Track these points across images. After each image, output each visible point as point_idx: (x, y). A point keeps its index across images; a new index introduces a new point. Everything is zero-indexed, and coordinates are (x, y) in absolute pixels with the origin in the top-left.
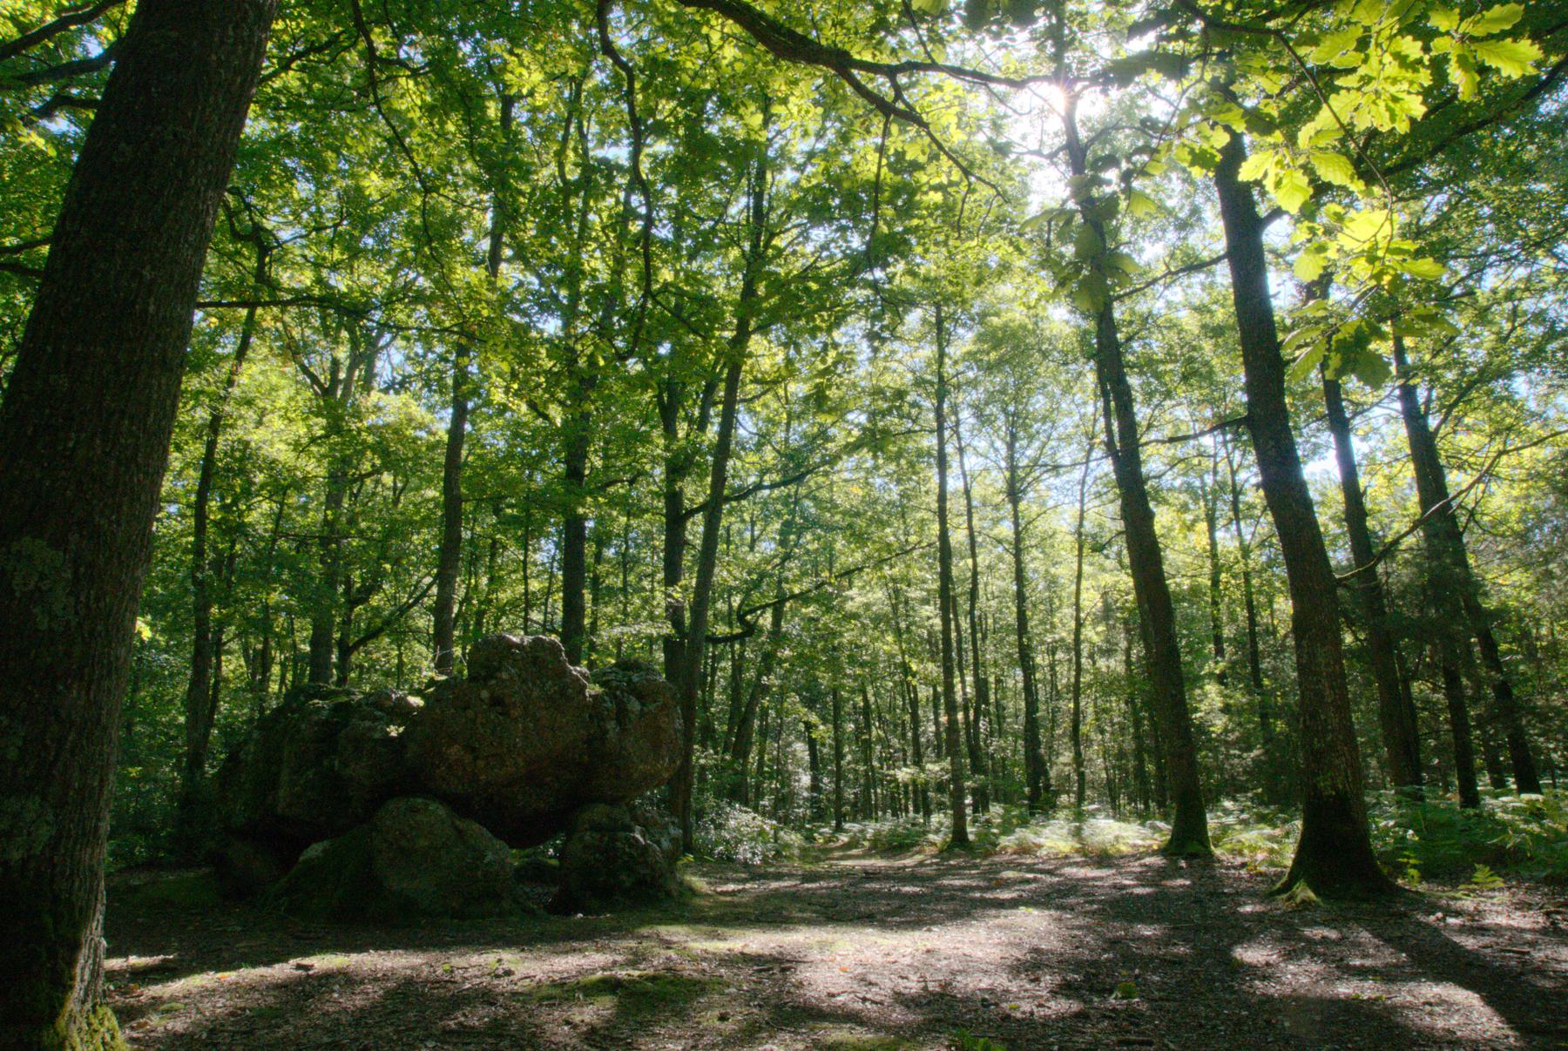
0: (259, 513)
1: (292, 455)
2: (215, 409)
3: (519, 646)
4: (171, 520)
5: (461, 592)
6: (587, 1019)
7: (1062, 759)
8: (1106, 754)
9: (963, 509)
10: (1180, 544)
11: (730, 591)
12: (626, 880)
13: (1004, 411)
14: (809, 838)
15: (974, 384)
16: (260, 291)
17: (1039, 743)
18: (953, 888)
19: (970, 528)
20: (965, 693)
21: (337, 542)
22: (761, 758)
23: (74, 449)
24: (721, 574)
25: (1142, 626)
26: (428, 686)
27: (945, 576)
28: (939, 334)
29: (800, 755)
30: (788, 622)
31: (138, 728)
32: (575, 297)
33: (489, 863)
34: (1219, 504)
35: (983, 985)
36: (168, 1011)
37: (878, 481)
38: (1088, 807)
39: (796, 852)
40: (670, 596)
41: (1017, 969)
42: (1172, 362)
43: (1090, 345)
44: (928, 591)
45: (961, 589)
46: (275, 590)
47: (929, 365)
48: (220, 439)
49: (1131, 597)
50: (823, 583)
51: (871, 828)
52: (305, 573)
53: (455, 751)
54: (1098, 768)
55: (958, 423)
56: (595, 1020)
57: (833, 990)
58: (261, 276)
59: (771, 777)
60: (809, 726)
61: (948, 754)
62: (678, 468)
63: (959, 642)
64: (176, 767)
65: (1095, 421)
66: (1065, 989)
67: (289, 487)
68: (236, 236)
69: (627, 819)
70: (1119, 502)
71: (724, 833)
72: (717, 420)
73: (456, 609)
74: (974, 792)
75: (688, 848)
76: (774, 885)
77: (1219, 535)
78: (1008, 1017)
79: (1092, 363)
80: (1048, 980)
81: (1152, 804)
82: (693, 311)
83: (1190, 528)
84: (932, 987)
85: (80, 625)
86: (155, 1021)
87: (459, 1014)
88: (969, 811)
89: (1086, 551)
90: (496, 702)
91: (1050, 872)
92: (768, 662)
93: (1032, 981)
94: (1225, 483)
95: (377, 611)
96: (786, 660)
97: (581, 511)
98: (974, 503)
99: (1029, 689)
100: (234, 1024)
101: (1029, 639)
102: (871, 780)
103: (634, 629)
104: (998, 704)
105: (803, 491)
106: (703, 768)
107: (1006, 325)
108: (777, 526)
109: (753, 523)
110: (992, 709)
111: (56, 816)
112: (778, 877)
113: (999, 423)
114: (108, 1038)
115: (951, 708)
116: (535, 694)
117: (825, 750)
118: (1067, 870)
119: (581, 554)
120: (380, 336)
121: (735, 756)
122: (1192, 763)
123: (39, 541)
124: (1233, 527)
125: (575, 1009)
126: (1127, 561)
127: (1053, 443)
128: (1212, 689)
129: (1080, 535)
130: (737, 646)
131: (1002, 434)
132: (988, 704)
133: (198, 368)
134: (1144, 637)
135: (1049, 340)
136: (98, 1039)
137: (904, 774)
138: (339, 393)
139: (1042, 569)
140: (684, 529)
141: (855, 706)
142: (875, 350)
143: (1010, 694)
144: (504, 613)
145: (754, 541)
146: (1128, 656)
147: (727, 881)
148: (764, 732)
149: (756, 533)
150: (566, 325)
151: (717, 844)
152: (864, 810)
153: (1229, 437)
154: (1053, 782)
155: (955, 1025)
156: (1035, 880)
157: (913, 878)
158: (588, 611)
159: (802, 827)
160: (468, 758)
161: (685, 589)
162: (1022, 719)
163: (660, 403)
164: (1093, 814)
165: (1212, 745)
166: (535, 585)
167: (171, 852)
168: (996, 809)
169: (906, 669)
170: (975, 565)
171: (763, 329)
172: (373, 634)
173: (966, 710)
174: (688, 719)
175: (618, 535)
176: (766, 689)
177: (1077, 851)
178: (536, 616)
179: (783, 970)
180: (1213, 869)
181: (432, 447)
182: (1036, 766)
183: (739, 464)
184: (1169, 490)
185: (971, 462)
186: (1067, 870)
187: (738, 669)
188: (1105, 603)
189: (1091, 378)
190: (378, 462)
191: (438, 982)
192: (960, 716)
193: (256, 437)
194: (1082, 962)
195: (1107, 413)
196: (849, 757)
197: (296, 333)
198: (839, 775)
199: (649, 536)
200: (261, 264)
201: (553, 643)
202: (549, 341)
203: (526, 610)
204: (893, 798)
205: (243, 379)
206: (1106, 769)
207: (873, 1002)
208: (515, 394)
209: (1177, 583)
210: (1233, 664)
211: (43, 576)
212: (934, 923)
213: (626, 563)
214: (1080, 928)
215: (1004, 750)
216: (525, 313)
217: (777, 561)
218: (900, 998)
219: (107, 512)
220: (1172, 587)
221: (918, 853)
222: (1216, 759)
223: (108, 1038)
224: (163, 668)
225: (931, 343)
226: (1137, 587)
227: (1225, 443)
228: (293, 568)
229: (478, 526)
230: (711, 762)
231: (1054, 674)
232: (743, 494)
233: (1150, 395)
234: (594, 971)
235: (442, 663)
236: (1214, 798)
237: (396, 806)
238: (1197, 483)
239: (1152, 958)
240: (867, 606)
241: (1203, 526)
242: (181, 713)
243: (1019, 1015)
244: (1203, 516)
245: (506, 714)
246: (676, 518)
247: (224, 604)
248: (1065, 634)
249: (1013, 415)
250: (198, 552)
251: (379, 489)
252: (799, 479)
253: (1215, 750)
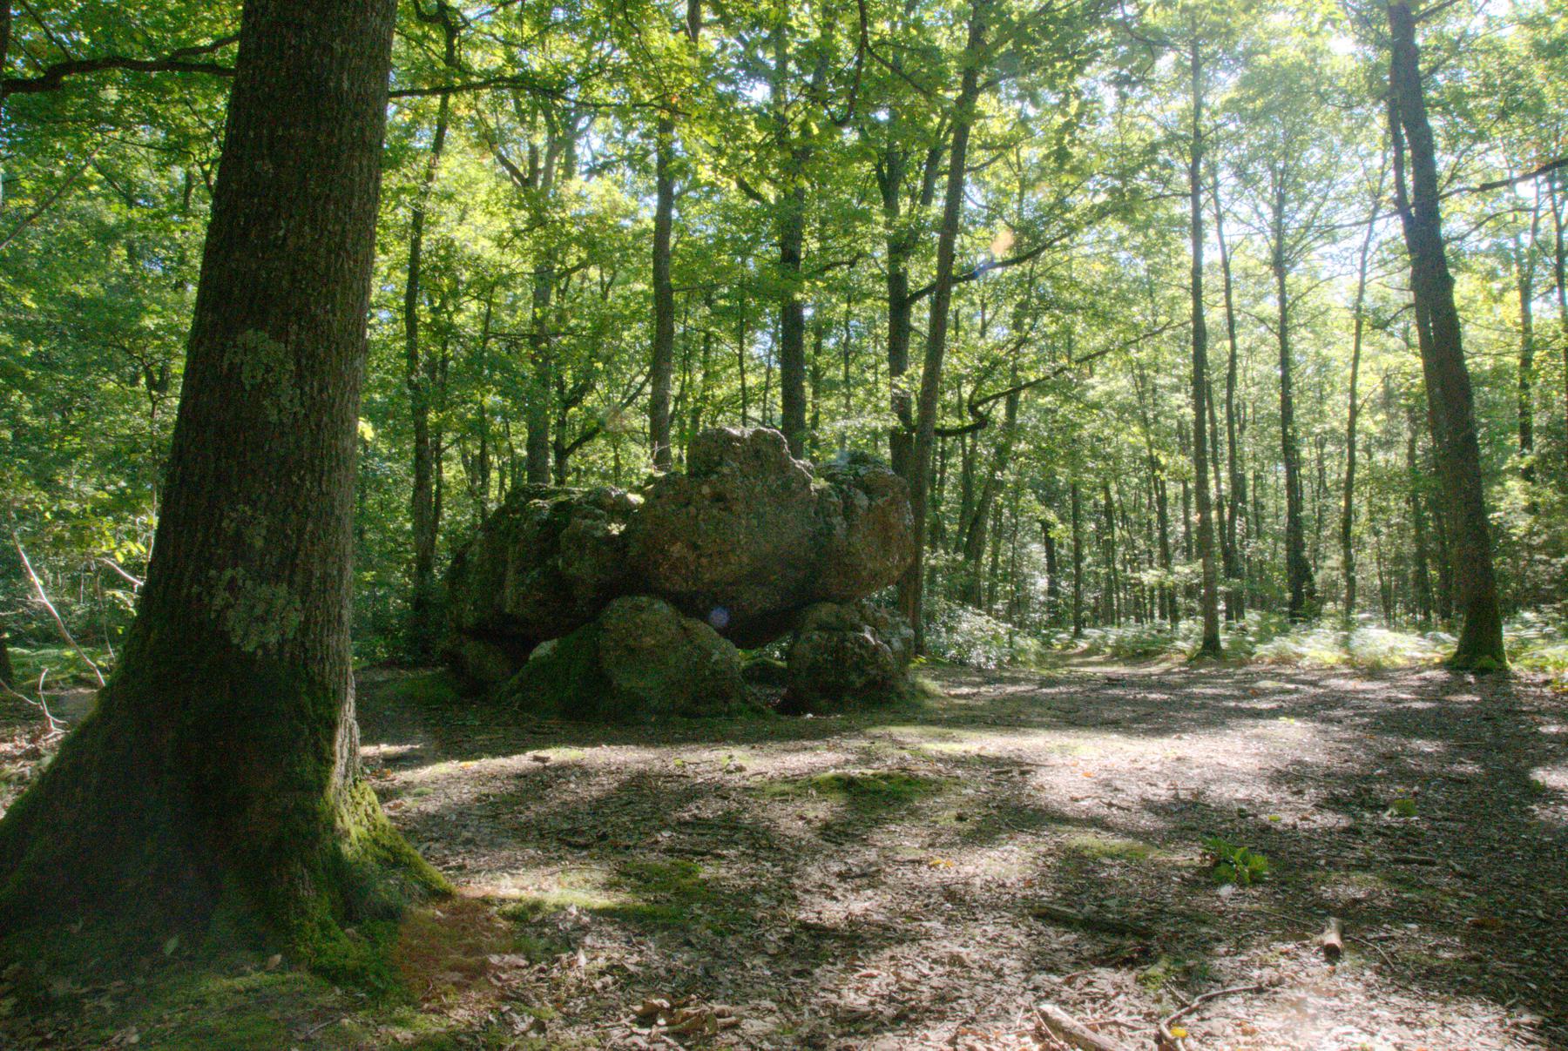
0: (468, 314)
1: (495, 251)
2: (418, 206)
3: (738, 439)
4: (383, 325)
5: (675, 390)
6: (821, 815)
7: (1329, 563)
8: (1381, 557)
9: (1221, 284)
10: (1484, 317)
11: (959, 380)
12: (858, 681)
13: (1272, 168)
14: (1047, 644)
15: (1236, 138)
16: (450, 78)
17: (1303, 546)
18: (1204, 696)
19: (1229, 305)
20: (1219, 490)
21: (548, 341)
22: (995, 560)
23: (285, 238)
24: (951, 363)
25: (1431, 414)
26: (647, 483)
27: (1199, 359)
28: (1195, 81)
29: (1035, 556)
30: (1023, 414)
31: (369, 536)
32: (783, 60)
33: (716, 663)
34: (1538, 269)
35: (1239, 796)
36: (419, 795)
37: (1123, 255)
38: (1357, 616)
39: (1032, 657)
40: (896, 386)
41: (1279, 778)
42: (1488, 95)
43: (1381, 82)
44: (1179, 377)
45: (1216, 375)
46: (489, 391)
47: (1183, 118)
48: (424, 239)
49: (1418, 381)
50: (1062, 369)
51: (1113, 634)
52: (517, 374)
53: (677, 549)
54: (1370, 574)
55: (1216, 185)
56: (829, 817)
57: (1076, 795)
58: (450, 59)
59: (1005, 580)
60: (1046, 526)
61: (1198, 557)
62: (901, 248)
63: (1214, 434)
64: (407, 573)
65: (1383, 174)
66: (1333, 803)
67: (496, 284)
68: (423, 18)
69: (857, 619)
70: (1410, 270)
71: (957, 637)
72: (942, 193)
73: (671, 408)
74: (1228, 597)
75: (920, 649)
76: (1010, 689)
77: (1535, 306)
78: (1269, 828)
79: (1382, 104)
80: (1311, 793)
81: (1433, 615)
82: (912, 68)
83: (1498, 298)
84: (1183, 795)
85: (306, 416)
86: (408, 802)
87: (692, 806)
88: (1221, 617)
89: (1365, 327)
90: (718, 498)
91: (1314, 684)
92: (1002, 456)
93: (1295, 793)
94: (1548, 243)
95: (591, 412)
96: (1022, 454)
97: (798, 296)
98: (1233, 277)
99: (1293, 487)
100: (479, 808)
101: (1295, 430)
102: (1113, 584)
103: (856, 422)
104: (1258, 505)
105: (1039, 269)
106: (934, 569)
107: (1276, 64)
108: (1011, 309)
109: (984, 306)
110: (1249, 508)
111: (303, 603)
112: (1014, 681)
113: (1263, 184)
114: (370, 811)
115: (1204, 506)
116: (758, 489)
117: (1063, 552)
118: (1333, 682)
119: (799, 344)
120: (576, 120)
121: (968, 557)
122: (1488, 568)
123: (260, 333)
124: (1555, 296)
125: (808, 805)
126: (1415, 339)
127: (1328, 204)
128: (1514, 485)
129: (1359, 309)
130: (968, 440)
131: (1268, 196)
132: (1244, 502)
133: (395, 164)
134: (1433, 428)
135: (1330, 79)
136: (361, 811)
137: (1150, 577)
138: (540, 183)
139: (1312, 350)
140: (909, 314)
141: (1096, 505)
142: (1124, 97)
143: (1270, 491)
144: (721, 411)
145: (985, 326)
146: (1412, 448)
147: (961, 684)
148: (998, 533)
149: (988, 317)
150: (776, 90)
151: (948, 648)
152: (1106, 615)
153: (1557, 185)
154: (1318, 587)
155: (1209, 834)
156: (1296, 691)
157: (1161, 685)
158: (809, 406)
159: (1039, 633)
160: (691, 556)
161: (911, 379)
162: (1284, 519)
163: (880, 176)
164: (1363, 624)
165: (1511, 549)
166: (752, 380)
167: (409, 653)
168: (1252, 617)
169: (1154, 463)
170: (1234, 348)
171: (991, 85)
172: (588, 436)
173: (1220, 507)
174: (919, 514)
175: (839, 323)
176: (1000, 485)
177: (1345, 662)
178: (753, 412)
179: (1023, 773)
180: (1508, 685)
181: (638, 236)
182: (1299, 571)
183: (967, 241)
184: (1474, 254)
185: (1231, 229)
186: (1333, 682)
187: (969, 464)
188: (1387, 387)
189: (1380, 123)
190: (584, 255)
191: (670, 777)
192: (1214, 514)
193: (461, 234)
194: (1352, 776)
195: (1399, 165)
196: (1089, 559)
197: (492, 123)
198: (1078, 578)
199: (871, 323)
200: (450, 47)
201: (774, 436)
202: (758, 110)
203: (743, 406)
204: (1137, 604)
205: (442, 173)
206: (1380, 575)
207: (1119, 808)
208: (724, 171)
209: (1478, 363)
210: (1543, 458)
211: (268, 369)
212: (1184, 731)
213: (847, 353)
214: (1348, 741)
215: (1262, 552)
216: (729, 80)
217: (1011, 346)
218: (1149, 806)
219: (322, 302)
220: (1471, 368)
221: (1163, 660)
222: (1515, 565)
223: (370, 811)
224: (387, 477)
225: (1185, 92)
226: (1427, 368)
227: (1552, 192)
228: (505, 369)
229: (691, 319)
230: (941, 563)
231: (1322, 471)
232: (971, 275)
233: (1453, 140)
234: (826, 769)
235: (661, 459)
236: (1512, 607)
237: (620, 605)
238: (1511, 245)
239: (1433, 775)
240: (1110, 395)
241: (1514, 296)
242: (409, 521)
243: (1280, 827)
244: (1515, 284)
245: (728, 509)
246: (900, 303)
247: (441, 408)
248: (1338, 424)
249: (1282, 172)
250: (411, 355)
251: (586, 285)
252: (1033, 255)
253: (1514, 556)
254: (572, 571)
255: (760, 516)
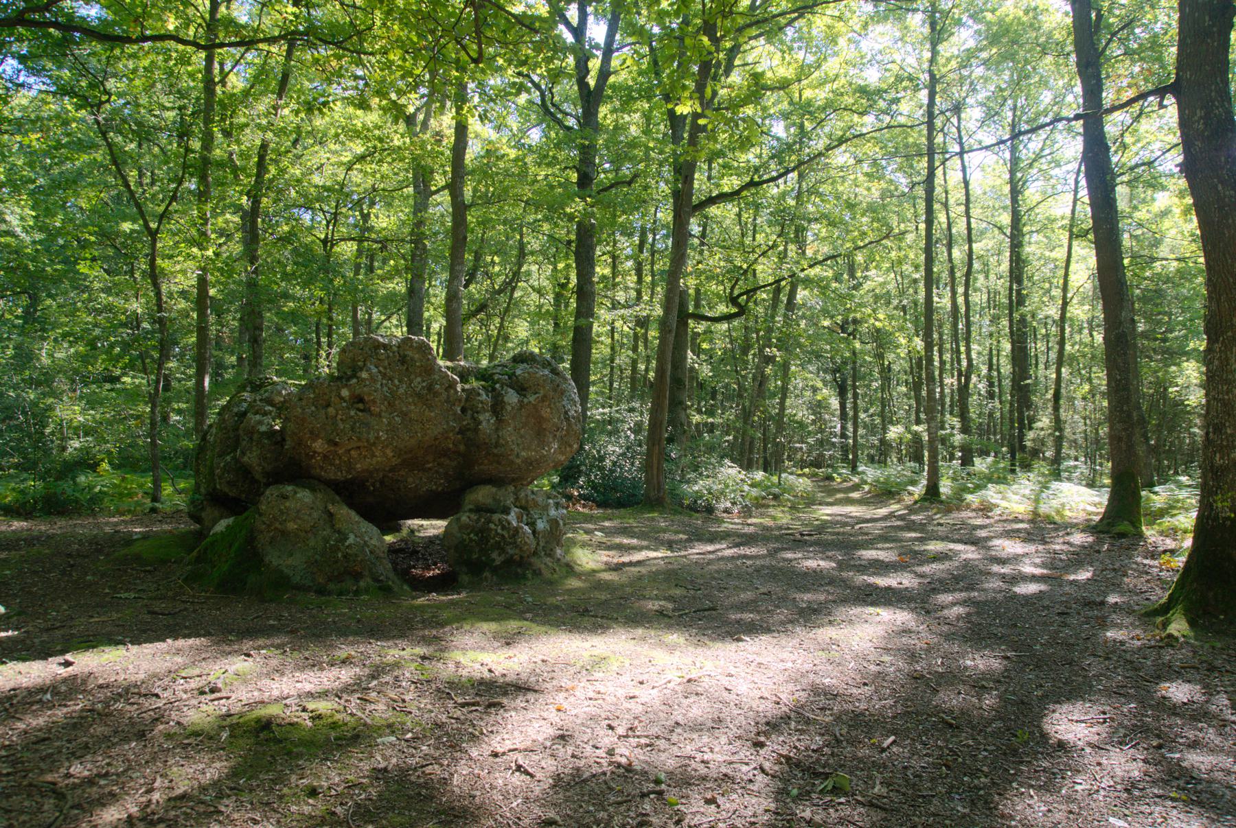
7: (1039, 425)
12: (497, 558)
116: (401, 391)
254: (245, 459)
255: (404, 415)
